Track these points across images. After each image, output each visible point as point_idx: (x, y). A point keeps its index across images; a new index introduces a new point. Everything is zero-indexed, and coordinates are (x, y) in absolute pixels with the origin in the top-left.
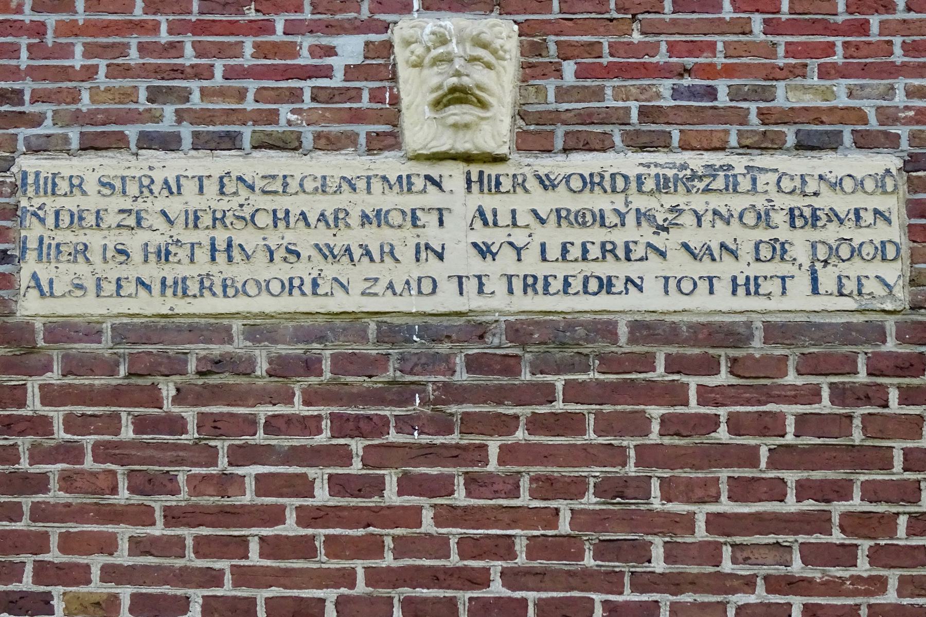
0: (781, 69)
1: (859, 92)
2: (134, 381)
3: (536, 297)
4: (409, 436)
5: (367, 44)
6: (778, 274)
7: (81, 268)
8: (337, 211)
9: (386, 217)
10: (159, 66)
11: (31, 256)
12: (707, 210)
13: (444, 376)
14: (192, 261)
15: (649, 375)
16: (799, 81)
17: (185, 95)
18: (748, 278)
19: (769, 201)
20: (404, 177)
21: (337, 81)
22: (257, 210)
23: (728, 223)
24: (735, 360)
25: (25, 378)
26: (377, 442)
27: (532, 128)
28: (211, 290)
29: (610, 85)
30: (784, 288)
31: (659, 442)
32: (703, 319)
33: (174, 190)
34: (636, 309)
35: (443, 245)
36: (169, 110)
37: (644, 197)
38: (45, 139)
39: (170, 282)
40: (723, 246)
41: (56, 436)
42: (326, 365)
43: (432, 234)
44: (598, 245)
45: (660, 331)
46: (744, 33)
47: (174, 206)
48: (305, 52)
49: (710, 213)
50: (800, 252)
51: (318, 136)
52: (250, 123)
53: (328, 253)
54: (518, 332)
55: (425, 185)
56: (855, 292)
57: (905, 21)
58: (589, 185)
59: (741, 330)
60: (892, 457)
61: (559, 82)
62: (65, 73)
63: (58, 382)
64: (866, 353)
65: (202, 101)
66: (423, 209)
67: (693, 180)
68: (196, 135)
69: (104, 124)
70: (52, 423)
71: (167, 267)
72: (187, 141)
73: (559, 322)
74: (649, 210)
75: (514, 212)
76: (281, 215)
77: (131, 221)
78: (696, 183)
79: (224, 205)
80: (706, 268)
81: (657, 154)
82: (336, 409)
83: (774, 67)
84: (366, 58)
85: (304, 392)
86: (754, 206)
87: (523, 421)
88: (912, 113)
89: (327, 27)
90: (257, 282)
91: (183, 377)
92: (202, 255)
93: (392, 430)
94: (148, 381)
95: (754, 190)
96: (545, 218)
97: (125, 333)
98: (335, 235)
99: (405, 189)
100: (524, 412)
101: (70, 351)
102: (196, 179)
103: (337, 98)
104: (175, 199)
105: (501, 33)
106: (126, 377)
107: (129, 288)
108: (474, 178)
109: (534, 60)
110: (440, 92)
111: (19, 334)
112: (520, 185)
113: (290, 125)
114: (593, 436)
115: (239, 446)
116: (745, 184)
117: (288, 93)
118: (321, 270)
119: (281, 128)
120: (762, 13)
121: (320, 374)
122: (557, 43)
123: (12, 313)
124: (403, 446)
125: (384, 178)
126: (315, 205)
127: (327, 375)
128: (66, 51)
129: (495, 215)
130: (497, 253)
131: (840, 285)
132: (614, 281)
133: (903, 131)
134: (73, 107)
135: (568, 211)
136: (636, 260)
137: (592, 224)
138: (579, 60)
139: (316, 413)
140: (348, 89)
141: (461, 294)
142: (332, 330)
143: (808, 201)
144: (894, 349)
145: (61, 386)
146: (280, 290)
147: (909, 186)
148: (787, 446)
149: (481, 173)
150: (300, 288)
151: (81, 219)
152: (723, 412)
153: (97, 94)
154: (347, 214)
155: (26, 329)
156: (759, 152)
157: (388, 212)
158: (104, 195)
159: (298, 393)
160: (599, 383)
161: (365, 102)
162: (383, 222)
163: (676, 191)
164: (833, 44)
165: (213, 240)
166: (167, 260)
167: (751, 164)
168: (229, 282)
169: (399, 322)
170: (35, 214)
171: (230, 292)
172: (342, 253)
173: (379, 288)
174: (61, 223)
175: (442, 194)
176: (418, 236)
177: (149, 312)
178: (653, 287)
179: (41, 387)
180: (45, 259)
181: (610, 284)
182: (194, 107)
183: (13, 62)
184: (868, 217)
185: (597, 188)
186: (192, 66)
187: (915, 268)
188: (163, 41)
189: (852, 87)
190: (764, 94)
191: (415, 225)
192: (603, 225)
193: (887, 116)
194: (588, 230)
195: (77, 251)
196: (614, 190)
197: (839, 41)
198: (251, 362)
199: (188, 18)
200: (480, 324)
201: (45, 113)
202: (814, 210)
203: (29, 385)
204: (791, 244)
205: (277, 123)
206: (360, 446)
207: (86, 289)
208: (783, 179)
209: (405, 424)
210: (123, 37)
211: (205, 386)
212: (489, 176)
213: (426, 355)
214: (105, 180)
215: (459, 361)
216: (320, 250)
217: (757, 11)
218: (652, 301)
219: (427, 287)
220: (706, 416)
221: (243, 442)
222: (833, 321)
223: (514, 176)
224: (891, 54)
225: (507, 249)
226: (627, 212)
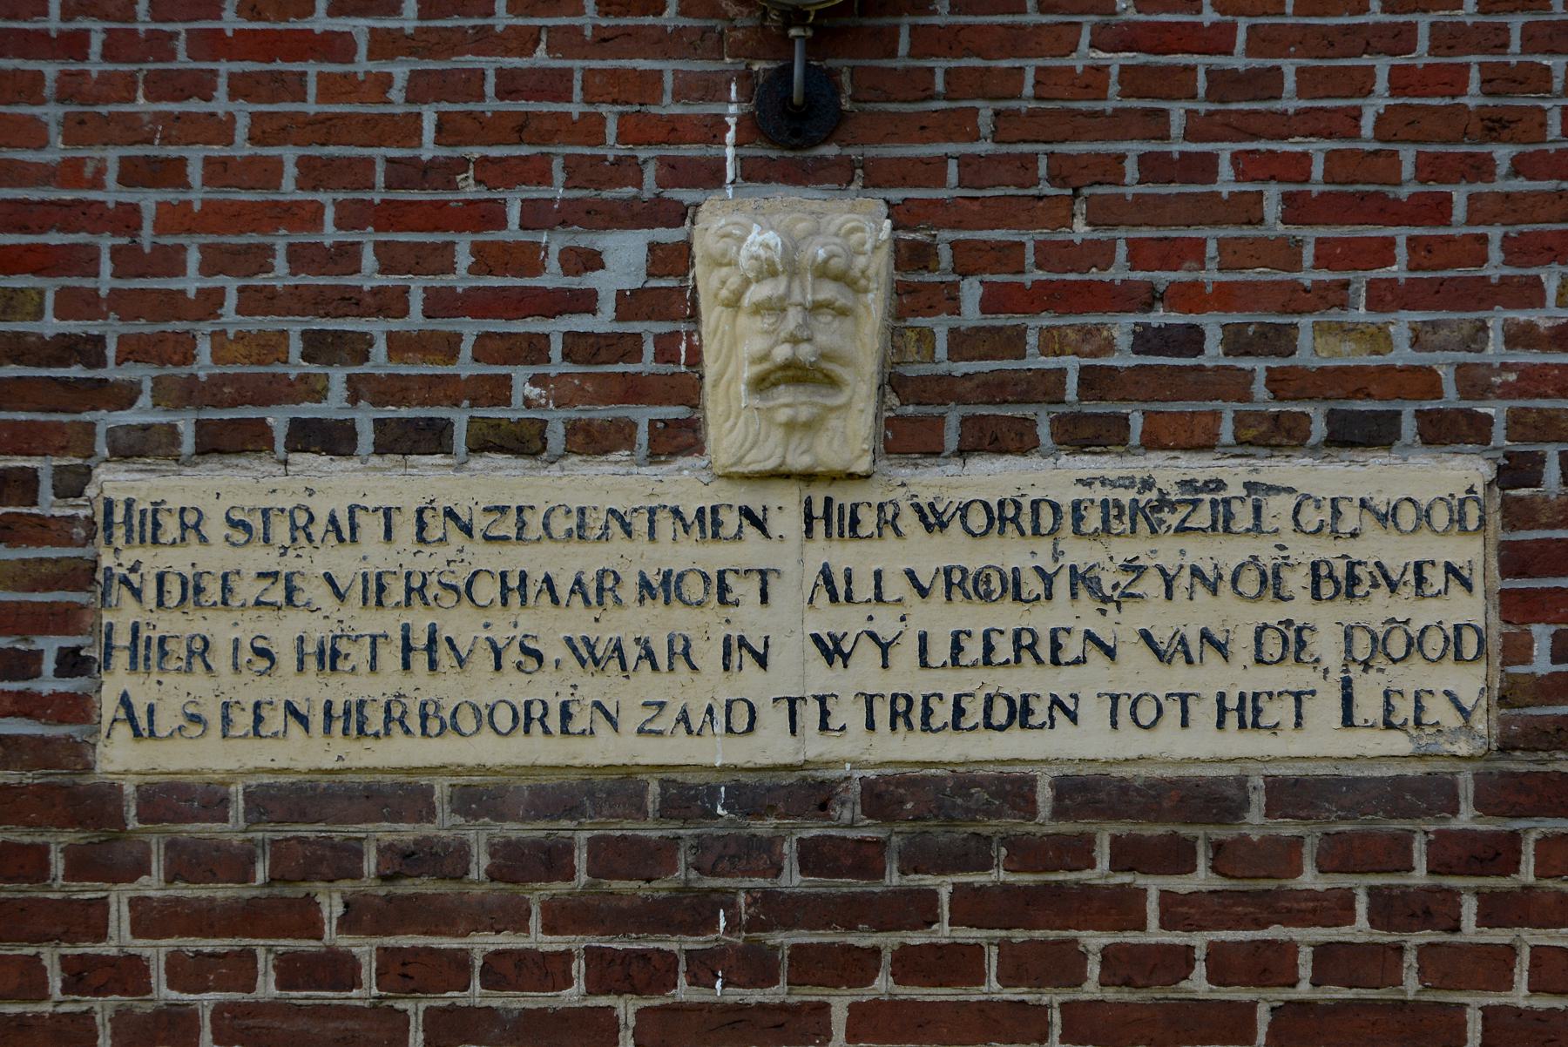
0: (1306, 291)
1: (1430, 337)
2: (277, 890)
3: (910, 735)
4: (706, 990)
5: (653, 247)
6: (1291, 689)
7: (198, 683)
8: (601, 575)
9: (678, 588)
10: (321, 290)
11: (121, 659)
12: (1181, 567)
13: (764, 877)
14: (373, 668)
15: (1086, 876)
16: (1334, 315)
17: (359, 348)
18: (1242, 697)
19: (1281, 547)
20: (708, 511)
21: (603, 322)
22: (475, 574)
23: (1215, 592)
24: (1218, 847)
25: (106, 886)
26: (657, 1001)
27: (910, 409)
28: (402, 723)
29: (1036, 324)
30: (1299, 716)
31: (1098, 996)
32: (1170, 773)
33: (346, 534)
34: (1066, 757)
35: (767, 638)
36: (338, 376)
37: (1084, 542)
38: (140, 433)
39: (338, 710)
40: (1205, 636)
41: (154, 995)
42: (581, 859)
43: (750, 619)
44: (1009, 636)
45: (1102, 796)
46: (1249, 223)
47: (346, 563)
48: (553, 264)
49: (1187, 572)
50: (1326, 646)
51: (573, 428)
52: (466, 403)
53: (585, 655)
54: (882, 796)
55: (740, 526)
56: (1411, 723)
57: (1508, 195)
58: (997, 523)
59: (1231, 792)
60: (1465, 1023)
61: (954, 321)
62: (172, 305)
63: (159, 894)
64: (1426, 833)
65: (390, 359)
66: (736, 572)
67: (1161, 510)
68: (379, 424)
69: (234, 404)
70: (147, 968)
71: (334, 680)
72: (366, 437)
73: (944, 779)
74: (1092, 567)
75: (878, 575)
76: (514, 582)
77: (277, 594)
78: (1165, 514)
79: (422, 563)
80: (1178, 677)
81: (1106, 458)
82: (595, 941)
83: (1296, 286)
84: (650, 275)
85: (546, 908)
86: (1255, 558)
87: (887, 958)
88: (1512, 377)
89: (589, 213)
90: (476, 709)
91: (356, 882)
92: (390, 657)
93: (682, 980)
94: (300, 890)
95: (1257, 528)
96: (927, 585)
97: (270, 801)
98: (597, 620)
99: (709, 533)
100: (888, 941)
101: (178, 836)
102: (381, 513)
103: (603, 354)
104: (348, 550)
105: (863, 245)
106: (267, 884)
107: (275, 719)
108: (818, 510)
109: (915, 278)
110: (766, 366)
111: (95, 806)
112: (889, 523)
113: (528, 407)
114: (996, 986)
115: (443, 1010)
116: (1243, 518)
117: (525, 345)
118: (575, 687)
119: (513, 413)
120: (1281, 181)
121: (570, 876)
122: (954, 245)
123: (89, 768)
124: (700, 1007)
125: (676, 512)
126: (568, 562)
127: (582, 878)
128: (171, 262)
129: (849, 581)
130: (850, 654)
131: (1389, 709)
132: (1033, 704)
133: (1494, 409)
134: (183, 371)
135: (964, 571)
136: (1068, 664)
137: (1001, 596)
138: (988, 277)
139: (563, 948)
140: (622, 335)
141: (793, 732)
142: (591, 794)
143: (1343, 547)
144: (1471, 826)
145: (163, 901)
146: (510, 725)
147: (1503, 517)
148: (1301, 1004)
149: (828, 501)
150: (542, 720)
151: (199, 590)
152: (1199, 941)
153: (222, 346)
154: (617, 579)
155: (111, 793)
156: (1267, 452)
157: (681, 576)
158: (233, 544)
159: (535, 909)
160: (1006, 888)
161: (648, 364)
162: (673, 595)
163: (1133, 531)
164: (1390, 243)
165: (406, 628)
166: (333, 668)
167: (1254, 478)
168: (431, 709)
169: (697, 781)
170: (125, 581)
171: (434, 726)
172: (609, 653)
173: (666, 721)
174: (167, 596)
175: (766, 541)
176: (728, 621)
177: (302, 765)
178: (1094, 712)
179: (134, 903)
180: (141, 667)
181: (1027, 711)
182: (377, 372)
183: (88, 283)
184: (1436, 578)
185: (1010, 527)
186: (376, 292)
187: (1508, 675)
188: (328, 242)
189: (1419, 326)
190: (1278, 340)
191: (722, 601)
192: (1017, 597)
193: (1474, 382)
194: (993, 605)
195: (191, 653)
196: (1036, 531)
197: (1401, 234)
198: (461, 852)
199: (367, 196)
200: (823, 782)
201: (140, 383)
202: (1351, 565)
203: (113, 899)
204: (1312, 629)
205: (507, 402)
206: (631, 1010)
207: (205, 724)
208: (1303, 508)
209: (702, 967)
210: (265, 234)
211: (389, 898)
212: (841, 507)
213: (737, 838)
214: (237, 516)
215: (789, 849)
216: (574, 650)
217: (1273, 178)
218: (1090, 743)
219: (741, 720)
220: (1172, 948)
221: (448, 1002)
222: (1377, 774)
223: (881, 507)
224: (1485, 260)
225: (867, 645)
226: (1056, 573)
